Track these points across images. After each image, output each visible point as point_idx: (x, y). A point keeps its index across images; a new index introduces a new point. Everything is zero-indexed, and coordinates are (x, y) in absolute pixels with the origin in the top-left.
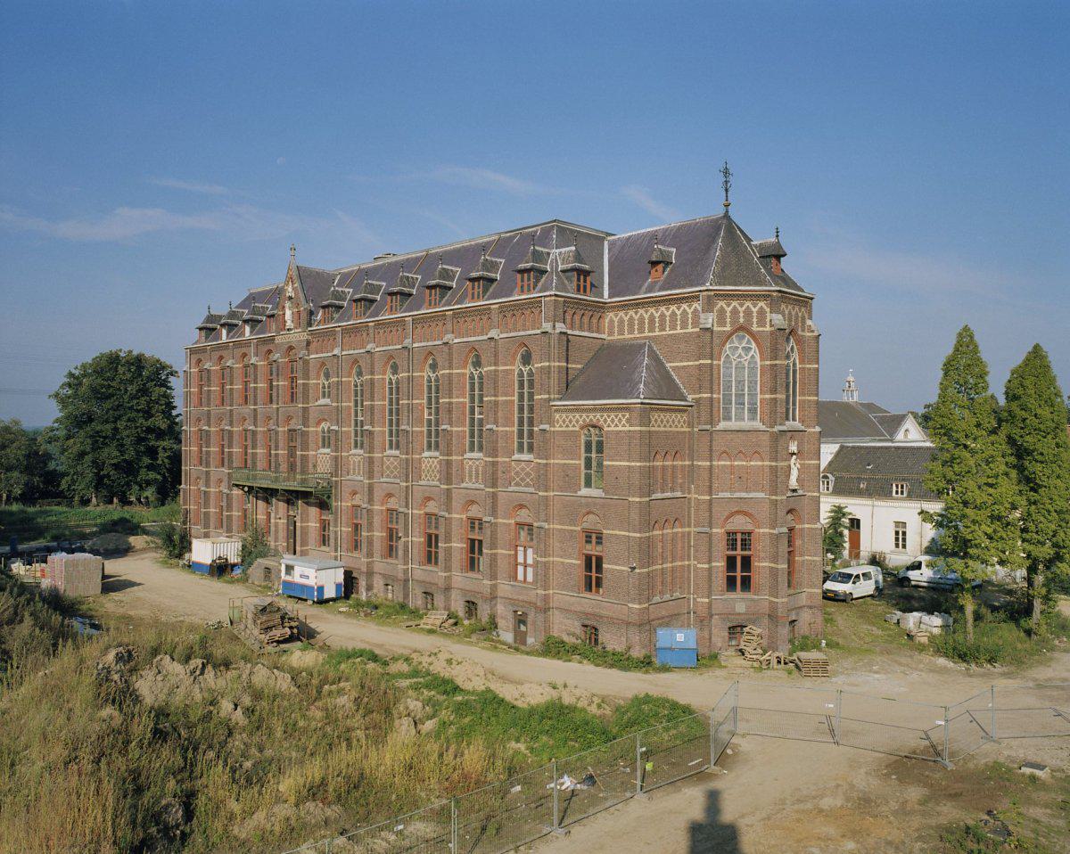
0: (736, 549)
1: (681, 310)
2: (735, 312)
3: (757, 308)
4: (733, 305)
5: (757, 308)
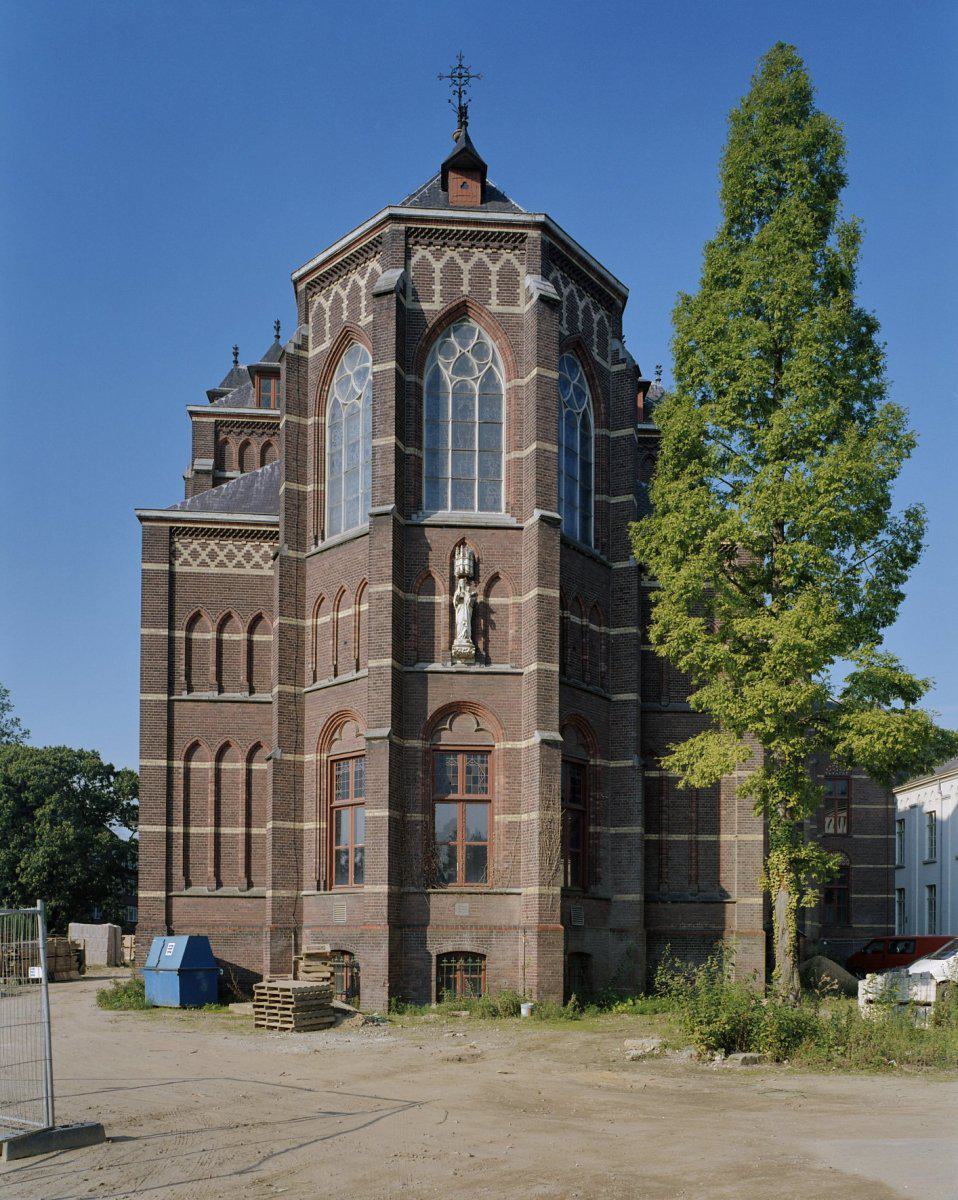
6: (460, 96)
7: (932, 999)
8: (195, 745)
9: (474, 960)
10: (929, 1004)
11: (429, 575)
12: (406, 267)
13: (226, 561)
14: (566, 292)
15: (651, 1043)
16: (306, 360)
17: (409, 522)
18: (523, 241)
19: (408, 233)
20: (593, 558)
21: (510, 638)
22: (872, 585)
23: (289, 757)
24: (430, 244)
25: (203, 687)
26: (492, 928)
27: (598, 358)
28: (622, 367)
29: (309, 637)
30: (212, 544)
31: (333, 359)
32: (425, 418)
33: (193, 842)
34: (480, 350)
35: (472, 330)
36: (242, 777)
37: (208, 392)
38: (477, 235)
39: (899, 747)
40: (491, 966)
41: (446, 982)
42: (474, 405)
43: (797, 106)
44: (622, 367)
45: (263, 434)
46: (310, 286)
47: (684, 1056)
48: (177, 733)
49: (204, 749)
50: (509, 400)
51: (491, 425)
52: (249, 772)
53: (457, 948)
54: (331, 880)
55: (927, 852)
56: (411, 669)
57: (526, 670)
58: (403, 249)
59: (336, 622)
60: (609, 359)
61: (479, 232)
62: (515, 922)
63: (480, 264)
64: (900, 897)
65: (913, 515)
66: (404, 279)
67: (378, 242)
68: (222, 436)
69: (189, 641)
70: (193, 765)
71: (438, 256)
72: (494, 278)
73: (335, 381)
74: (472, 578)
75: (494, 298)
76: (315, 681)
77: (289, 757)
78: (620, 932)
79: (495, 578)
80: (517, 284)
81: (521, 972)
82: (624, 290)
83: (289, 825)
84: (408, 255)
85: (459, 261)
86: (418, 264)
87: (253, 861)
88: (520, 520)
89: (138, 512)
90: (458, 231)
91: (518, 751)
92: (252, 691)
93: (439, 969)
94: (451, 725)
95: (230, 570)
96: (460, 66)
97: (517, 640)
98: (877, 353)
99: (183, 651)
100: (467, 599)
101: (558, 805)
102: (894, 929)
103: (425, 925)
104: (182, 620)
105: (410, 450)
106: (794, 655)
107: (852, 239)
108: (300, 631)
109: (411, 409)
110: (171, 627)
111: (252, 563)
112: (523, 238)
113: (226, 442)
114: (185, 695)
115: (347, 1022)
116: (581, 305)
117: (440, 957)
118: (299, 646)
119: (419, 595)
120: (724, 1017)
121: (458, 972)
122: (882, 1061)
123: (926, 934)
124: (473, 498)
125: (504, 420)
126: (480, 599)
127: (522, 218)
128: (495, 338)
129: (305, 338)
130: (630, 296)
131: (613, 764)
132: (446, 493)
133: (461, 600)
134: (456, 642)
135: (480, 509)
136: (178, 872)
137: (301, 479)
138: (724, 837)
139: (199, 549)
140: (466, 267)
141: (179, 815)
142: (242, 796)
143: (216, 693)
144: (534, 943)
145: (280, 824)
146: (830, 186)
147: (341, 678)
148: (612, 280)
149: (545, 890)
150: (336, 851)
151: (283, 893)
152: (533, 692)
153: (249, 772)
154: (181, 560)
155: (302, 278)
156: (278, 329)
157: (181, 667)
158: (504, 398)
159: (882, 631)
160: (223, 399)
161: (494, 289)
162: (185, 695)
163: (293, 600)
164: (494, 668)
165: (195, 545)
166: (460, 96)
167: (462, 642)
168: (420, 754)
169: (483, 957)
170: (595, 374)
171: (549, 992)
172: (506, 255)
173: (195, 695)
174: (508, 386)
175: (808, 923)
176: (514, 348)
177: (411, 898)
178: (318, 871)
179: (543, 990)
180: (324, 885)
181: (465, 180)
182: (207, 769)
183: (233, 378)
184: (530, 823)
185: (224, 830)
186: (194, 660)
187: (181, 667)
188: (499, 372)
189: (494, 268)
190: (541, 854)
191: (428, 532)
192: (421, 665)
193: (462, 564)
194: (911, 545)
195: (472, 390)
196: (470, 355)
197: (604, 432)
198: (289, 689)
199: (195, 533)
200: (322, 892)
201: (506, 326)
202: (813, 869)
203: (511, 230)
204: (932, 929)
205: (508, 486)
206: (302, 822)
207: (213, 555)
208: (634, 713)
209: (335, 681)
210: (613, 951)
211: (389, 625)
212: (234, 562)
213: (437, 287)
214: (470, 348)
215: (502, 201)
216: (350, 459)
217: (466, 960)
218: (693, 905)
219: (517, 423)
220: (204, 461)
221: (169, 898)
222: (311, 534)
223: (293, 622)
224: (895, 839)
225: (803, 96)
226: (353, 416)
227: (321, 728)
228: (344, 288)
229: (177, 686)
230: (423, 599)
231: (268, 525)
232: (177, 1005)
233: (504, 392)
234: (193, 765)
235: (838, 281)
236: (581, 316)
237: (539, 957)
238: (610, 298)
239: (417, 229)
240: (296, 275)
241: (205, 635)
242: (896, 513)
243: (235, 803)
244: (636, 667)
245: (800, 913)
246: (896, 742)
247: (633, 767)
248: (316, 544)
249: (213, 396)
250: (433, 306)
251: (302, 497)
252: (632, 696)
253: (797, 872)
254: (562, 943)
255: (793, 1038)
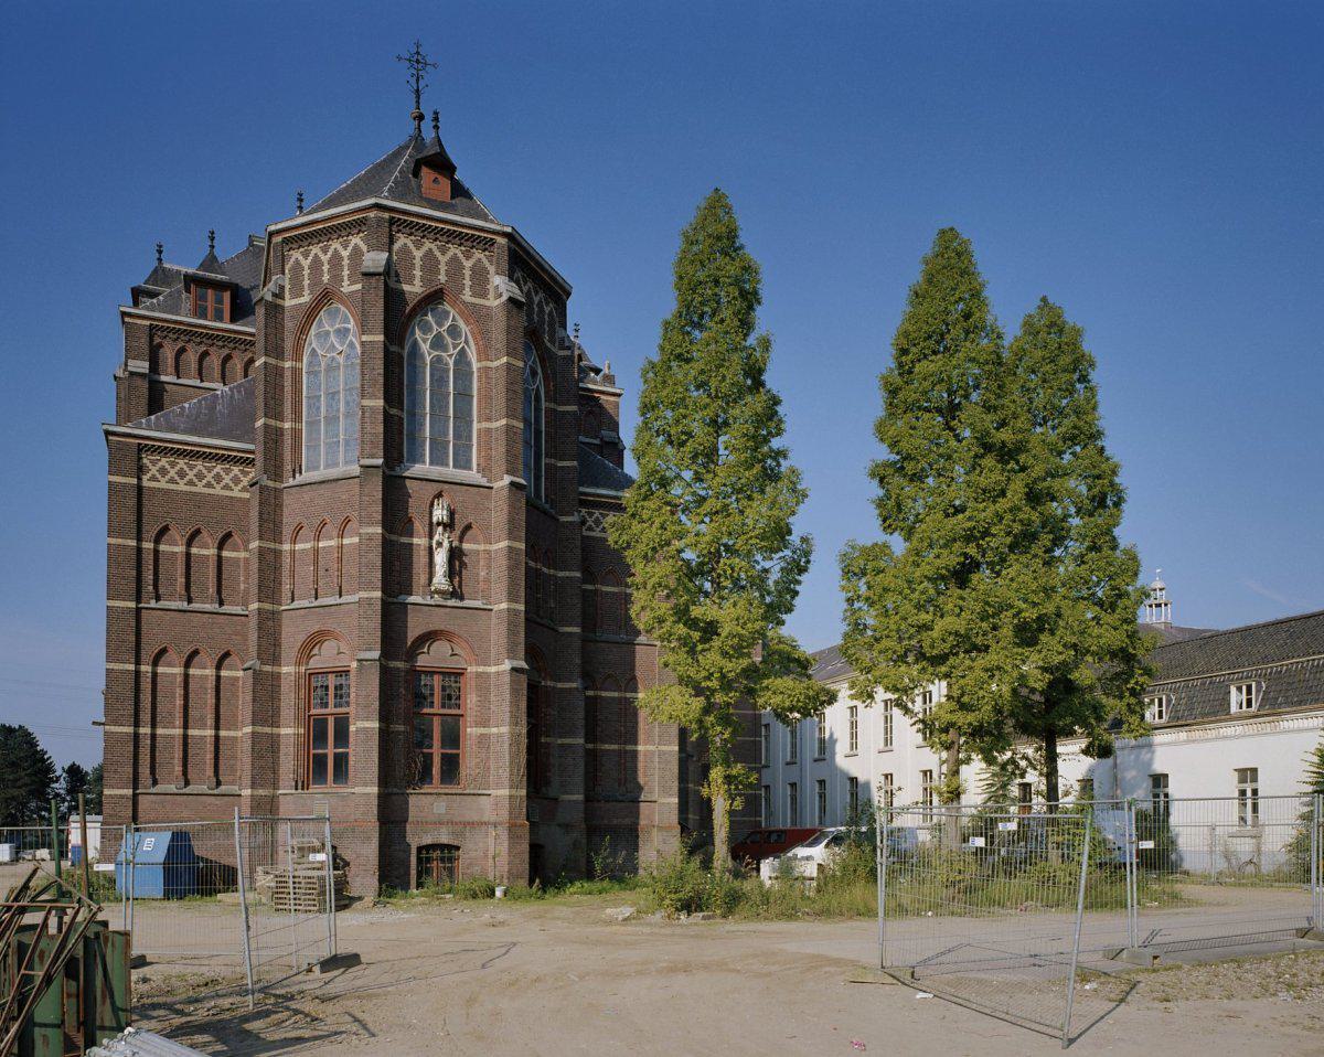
0: (326, 705)
1: (329, 254)
2: (316, 265)
3: (350, 248)
4: (333, 247)
5: (350, 248)
6: (418, 80)
7: (815, 875)
8: (163, 651)
9: (449, 851)
10: (812, 879)
11: (410, 520)
12: (390, 251)
13: (195, 480)
14: (525, 289)
15: (627, 911)
16: (283, 307)
17: (392, 473)
18: (492, 245)
19: (392, 221)
20: (545, 513)
21: (481, 579)
22: (776, 583)
23: (268, 668)
24: (411, 234)
25: (171, 597)
26: (466, 824)
27: (549, 344)
28: (568, 353)
29: (286, 561)
30: (181, 463)
31: (311, 313)
32: (405, 383)
33: (160, 743)
34: (454, 331)
35: (448, 313)
36: (211, 684)
37: (132, 289)
38: (452, 234)
39: (800, 704)
40: (464, 858)
41: (423, 872)
42: (448, 377)
43: (728, 242)
44: (568, 353)
45: (201, 343)
46: (286, 241)
47: (658, 917)
48: (144, 640)
49: (171, 655)
50: (480, 377)
51: (463, 396)
52: (218, 678)
53: (435, 841)
54: (308, 781)
55: (789, 754)
56: (395, 600)
57: (496, 608)
58: (386, 235)
59: (316, 551)
60: (557, 344)
61: (455, 231)
62: (485, 819)
63: (455, 258)
64: (766, 793)
65: (804, 540)
66: (389, 260)
67: (361, 223)
68: (157, 340)
69: (156, 552)
70: (160, 670)
71: (418, 245)
72: (467, 273)
73: (313, 331)
74: (449, 526)
75: (467, 289)
76: (293, 600)
77: (268, 668)
78: (567, 827)
79: (468, 527)
80: (487, 281)
81: (491, 861)
82: (567, 287)
83: (268, 730)
84: (392, 241)
85: (438, 254)
86: (400, 250)
87: (221, 762)
88: (489, 481)
89: (105, 427)
90: (436, 227)
91: (488, 675)
92: (221, 603)
93: (419, 860)
94: (429, 649)
95: (200, 488)
96: (418, 53)
97: (487, 580)
98: (781, 421)
99: (151, 562)
100: (446, 544)
101: (524, 722)
102: (760, 822)
103: (406, 821)
104: (150, 530)
105: (394, 411)
106: (736, 640)
107: (766, 344)
108: (278, 554)
109: (396, 375)
110: (139, 539)
111: (222, 484)
112: (492, 242)
113: (160, 346)
114: (153, 604)
115: (357, 905)
116: (536, 299)
117: (420, 849)
118: (277, 569)
119: (401, 536)
120: (688, 887)
121: (435, 862)
122: (790, 914)
123: (789, 826)
124: (448, 456)
125: (475, 393)
126: (456, 544)
127: (493, 226)
128: (467, 323)
129: (282, 288)
130: (573, 291)
131: (560, 685)
132: (424, 450)
133: (440, 544)
134: (435, 580)
135: (455, 466)
136: (145, 771)
137: (280, 417)
138: (640, 748)
139: (167, 466)
140: (443, 259)
141: (146, 716)
142: (211, 701)
143: (186, 603)
144: (505, 837)
145: (259, 729)
146: (750, 299)
147: (322, 601)
148: (561, 281)
149: (514, 792)
150: (314, 755)
151: (261, 792)
152: (503, 628)
153: (218, 678)
154: (149, 475)
155: (279, 232)
156: (212, 239)
157: (149, 576)
158: (475, 375)
159: (784, 617)
160: (155, 301)
161: (467, 282)
162: (153, 604)
163: (271, 526)
164: (467, 603)
165: (164, 462)
166: (418, 80)
167: (440, 579)
168: (403, 674)
169: (458, 848)
170: (545, 357)
171: (519, 876)
172: (478, 254)
173: (163, 604)
174: (479, 365)
175: (690, 816)
176: (483, 336)
177: (394, 798)
178: (295, 772)
179: (512, 876)
180: (301, 784)
181: (437, 175)
182: (175, 674)
183: (160, 275)
184: (500, 735)
185: (191, 732)
186: (161, 569)
187: (149, 576)
188: (471, 351)
189: (468, 264)
190: (511, 763)
191: (408, 482)
192: (402, 597)
193: (439, 513)
194: (803, 560)
195: (447, 364)
196: (445, 334)
197: (552, 406)
198: (267, 606)
199: (165, 452)
200: (300, 791)
201: (477, 316)
202: (740, 782)
203: (482, 234)
204: (794, 822)
205: (479, 451)
206: (278, 727)
207: (182, 474)
208: (577, 644)
209: (316, 603)
210: (560, 844)
211: (379, 563)
212: (204, 481)
213: (418, 273)
214: (446, 327)
215: (465, 197)
216: (329, 406)
217: (442, 852)
218: (623, 804)
219: (486, 398)
220: (139, 363)
221: (135, 796)
222: (288, 467)
223: (272, 546)
224: (761, 742)
225: (732, 235)
226: (332, 368)
227: (300, 644)
228: (325, 252)
229: (144, 595)
230: (404, 540)
231: (239, 451)
232: (161, 896)
233: (475, 370)
234: (160, 670)
235: (755, 374)
236: (547, 319)
237: (510, 848)
238: (556, 292)
239: (399, 219)
240: (272, 228)
241: (174, 548)
242: (794, 539)
243: (204, 703)
244: (579, 605)
245: (731, 813)
246: (798, 701)
247: (577, 688)
248: (294, 477)
249: (137, 294)
250: (414, 288)
251: (280, 432)
252: (577, 630)
253: (729, 784)
254: (527, 836)
255: (733, 902)
